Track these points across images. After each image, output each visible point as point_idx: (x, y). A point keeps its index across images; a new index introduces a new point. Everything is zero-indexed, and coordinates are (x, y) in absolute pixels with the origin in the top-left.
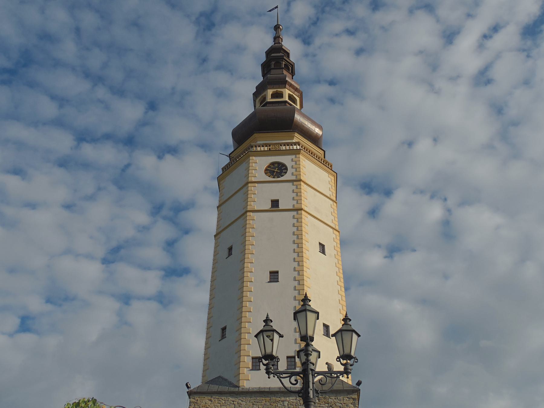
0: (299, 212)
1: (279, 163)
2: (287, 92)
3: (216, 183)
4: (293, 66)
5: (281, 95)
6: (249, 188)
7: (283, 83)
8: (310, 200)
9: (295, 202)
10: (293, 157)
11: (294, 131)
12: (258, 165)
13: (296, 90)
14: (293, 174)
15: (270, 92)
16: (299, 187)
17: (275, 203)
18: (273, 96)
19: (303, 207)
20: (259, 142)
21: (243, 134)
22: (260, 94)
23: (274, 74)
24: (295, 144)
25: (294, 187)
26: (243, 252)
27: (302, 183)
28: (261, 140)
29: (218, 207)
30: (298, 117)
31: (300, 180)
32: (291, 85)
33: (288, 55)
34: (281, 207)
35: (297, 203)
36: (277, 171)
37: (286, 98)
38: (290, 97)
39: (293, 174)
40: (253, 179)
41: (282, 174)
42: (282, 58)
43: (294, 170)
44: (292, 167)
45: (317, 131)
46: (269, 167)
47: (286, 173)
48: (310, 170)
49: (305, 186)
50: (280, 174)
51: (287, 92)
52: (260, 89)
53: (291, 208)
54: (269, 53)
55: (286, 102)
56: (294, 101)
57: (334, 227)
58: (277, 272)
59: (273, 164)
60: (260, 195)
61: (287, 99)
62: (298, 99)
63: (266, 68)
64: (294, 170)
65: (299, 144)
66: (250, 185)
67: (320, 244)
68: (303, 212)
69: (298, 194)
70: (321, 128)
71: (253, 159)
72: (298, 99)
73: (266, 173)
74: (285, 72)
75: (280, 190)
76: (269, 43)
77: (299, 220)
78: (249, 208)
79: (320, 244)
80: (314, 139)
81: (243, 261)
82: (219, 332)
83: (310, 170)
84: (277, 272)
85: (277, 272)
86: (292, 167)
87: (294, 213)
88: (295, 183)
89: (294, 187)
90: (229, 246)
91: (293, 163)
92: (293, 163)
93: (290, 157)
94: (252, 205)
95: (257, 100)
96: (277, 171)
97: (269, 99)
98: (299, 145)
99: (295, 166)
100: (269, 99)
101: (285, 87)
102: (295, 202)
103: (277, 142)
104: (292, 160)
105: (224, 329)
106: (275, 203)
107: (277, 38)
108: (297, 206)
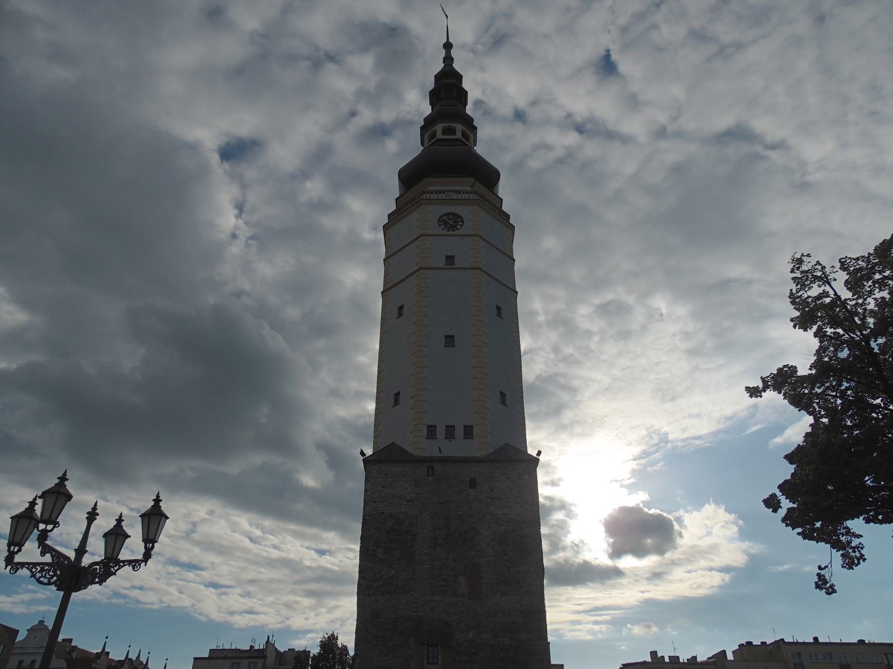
1: (454, 214)
3: (381, 236)
5: (452, 131)
17: (450, 259)
20: (430, 188)
28: (432, 185)
29: (382, 293)
37: (459, 135)
41: (459, 227)
50: (453, 228)
54: (438, 77)
58: (453, 257)
59: (448, 214)
76: (445, 41)
82: (392, 397)
84: (453, 336)
85: (453, 257)
95: (426, 136)
97: (439, 135)
100: (439, 135)
103: (448, 188)
105: (401, 308)
106: (450, 259)
107: (448, 60)
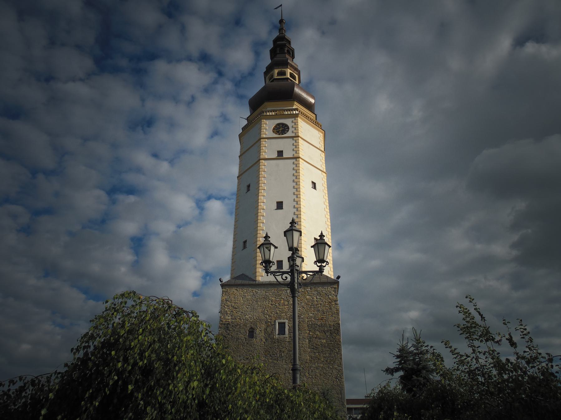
5: (284, 73)
6: (262, 143)
7: (285, 64)
8: (305, 150)
10: (293, 119)
11: (294, 100)
12: (267, 127)
13: (296, 69)
14: (293, 132)
15: (276, 71)
17: (280, 153)
19: (300, 156)
24: (295, 110)
26: (258, 189)
27: (300, 139)
31: (298, 136)
32: (292, 66)
34: (285, 156)
36: (281, 130)
39: (293, 132)
40: (264, 136)
42: (284, 45)
46: (275, 127)
52: (269, 69)
56: (294, 78)
62: (297, 76)
63: (273, 53)
64: (293, 129)
66: (261, 161)
67: (313, 182)
68: (300, 160)
69: (296, 147)
72: (297, 76)
73: (273, 132)
75: (284, 144)
77: (297, 165)
79: (313, 182)
81: (257, 195)
87: (294, 160)
88: (295, 139)
93: (291, 120)
94: (264, 155)
100: (276, 76)
106: (280, 153)
108: (296, 155)
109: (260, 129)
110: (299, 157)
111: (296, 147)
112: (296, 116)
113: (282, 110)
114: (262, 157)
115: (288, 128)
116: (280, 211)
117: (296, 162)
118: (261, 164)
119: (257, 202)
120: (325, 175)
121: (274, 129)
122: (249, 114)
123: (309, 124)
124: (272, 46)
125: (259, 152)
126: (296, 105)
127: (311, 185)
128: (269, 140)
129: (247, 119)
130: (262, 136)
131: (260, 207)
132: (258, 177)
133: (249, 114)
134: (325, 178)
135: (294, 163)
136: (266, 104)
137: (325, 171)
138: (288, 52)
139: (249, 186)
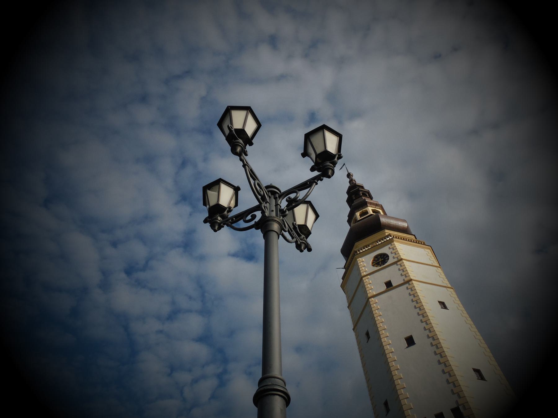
0: (410, 283)
2: (370, 209)
4: (368, 192)
5: (367, 212)
6: (365, 281)
7: (365, 204)
8: (413, 271)
9: (404, 277)
10: (390, 246)
11: (384, 229)
12: (365, 263)
13: (377, 205)
14: (394, 258)
15: (358, 214)
16: (402, 265)
17: (389, 284)
18: (361, 216)
19: (412, 278)
21: (348, 250)
22: (352, 219)
23: (356, 202)
24: (387, 236)
25: (399, 266)
26: (377, 332)
27: (404, 261)
30: (383, 220)
31: (402, 259)
32: (371, 203)
33: (362, 187)
34: (394, 284)
35: (406, 277)
36: (381, 260)
38: (373, 211)
39: (394, 258)
40: (365, 274)
42: (359, 191)
43: (393, 255)
44: (392, 253)
45: (405, 225)
46: (374, 260)
47: (388, 259)
48: (404, 249)
49: (434, 264)
50: (384, 262)
51: (370, 209)
52: (351, 216)
53: (258, 269)
55: (372, 215)
56: (379, 212)
57: (446, 285)
59: (376, 257)
60: (374, 284)
61: (372, 213)
62: (380, 211)
63: (350, 201)
64: (393, 255)
65: (390, 235)
66: (364, 279)
67: (440, 302)
68: (413, 282)
69: (404, 270)
70: (404, 221)
71: (360, 260)
72: (380, 211)
73: (373, 266)
74: (363, 198)
75: (389, 273)
77: (413, 289)
78: (369, 295)
79: (440, 302)
80: (405, 231)
81: (379, 339)
83: (404, 249)
86: (392, 253)
87: (407, 285)
88: (398, 263)
89: (399, 266)
90: (365, 332)
91: (391, 250)
92: (391, 250)
93: (387, 247)
94: (371, 293)
96: (381, 260)
98: (391, 236)
99: (393, 251)
100: (359, 218)
101: (367, 206)
102: (404, 277)
104: (390, 248)
106: (389, 284)
108: (406, 279)
109: (358, 269)
110: (411, 280)
111: (403, 271)
112: (391, 241)
113: (375, 242)
114: (369, 295)
115: (388, 256)
116: (387, 280)
117: (409, 287)
118: (371, 303)
119: (381, 346)
120: (452, 290)
121: (373, 263)
122: (345, 262)
123: (410, 245)
124: (349, 209)
125: (365, 292)
126: (387, 232)
127: (439, 306)
128: (372, 276)
129: (345, 268)
130: (362, 274)
131: (387, 352)
132: (373, 318)
133: (344, 262)
134: (454, 293)
135: (407, 288)
136: (356, 244)
137: (449, 286)
138: (364, 195)
139: (367, 334)
